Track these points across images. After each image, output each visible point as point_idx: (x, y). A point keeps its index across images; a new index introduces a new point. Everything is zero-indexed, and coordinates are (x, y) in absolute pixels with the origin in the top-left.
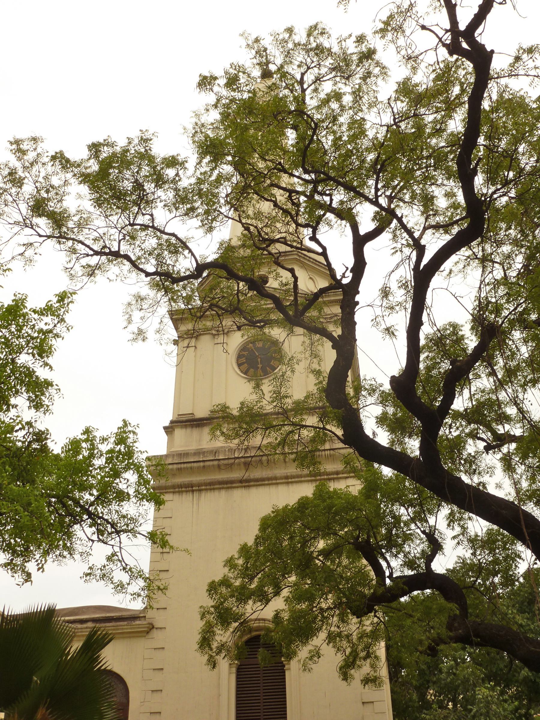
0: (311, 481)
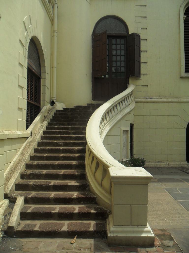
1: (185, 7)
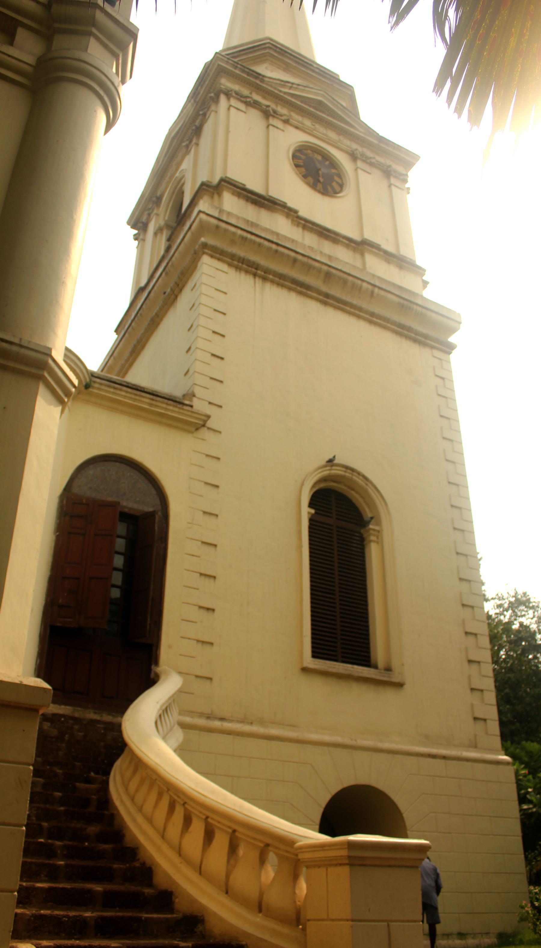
0: (195, 413)
1: (313, 487)
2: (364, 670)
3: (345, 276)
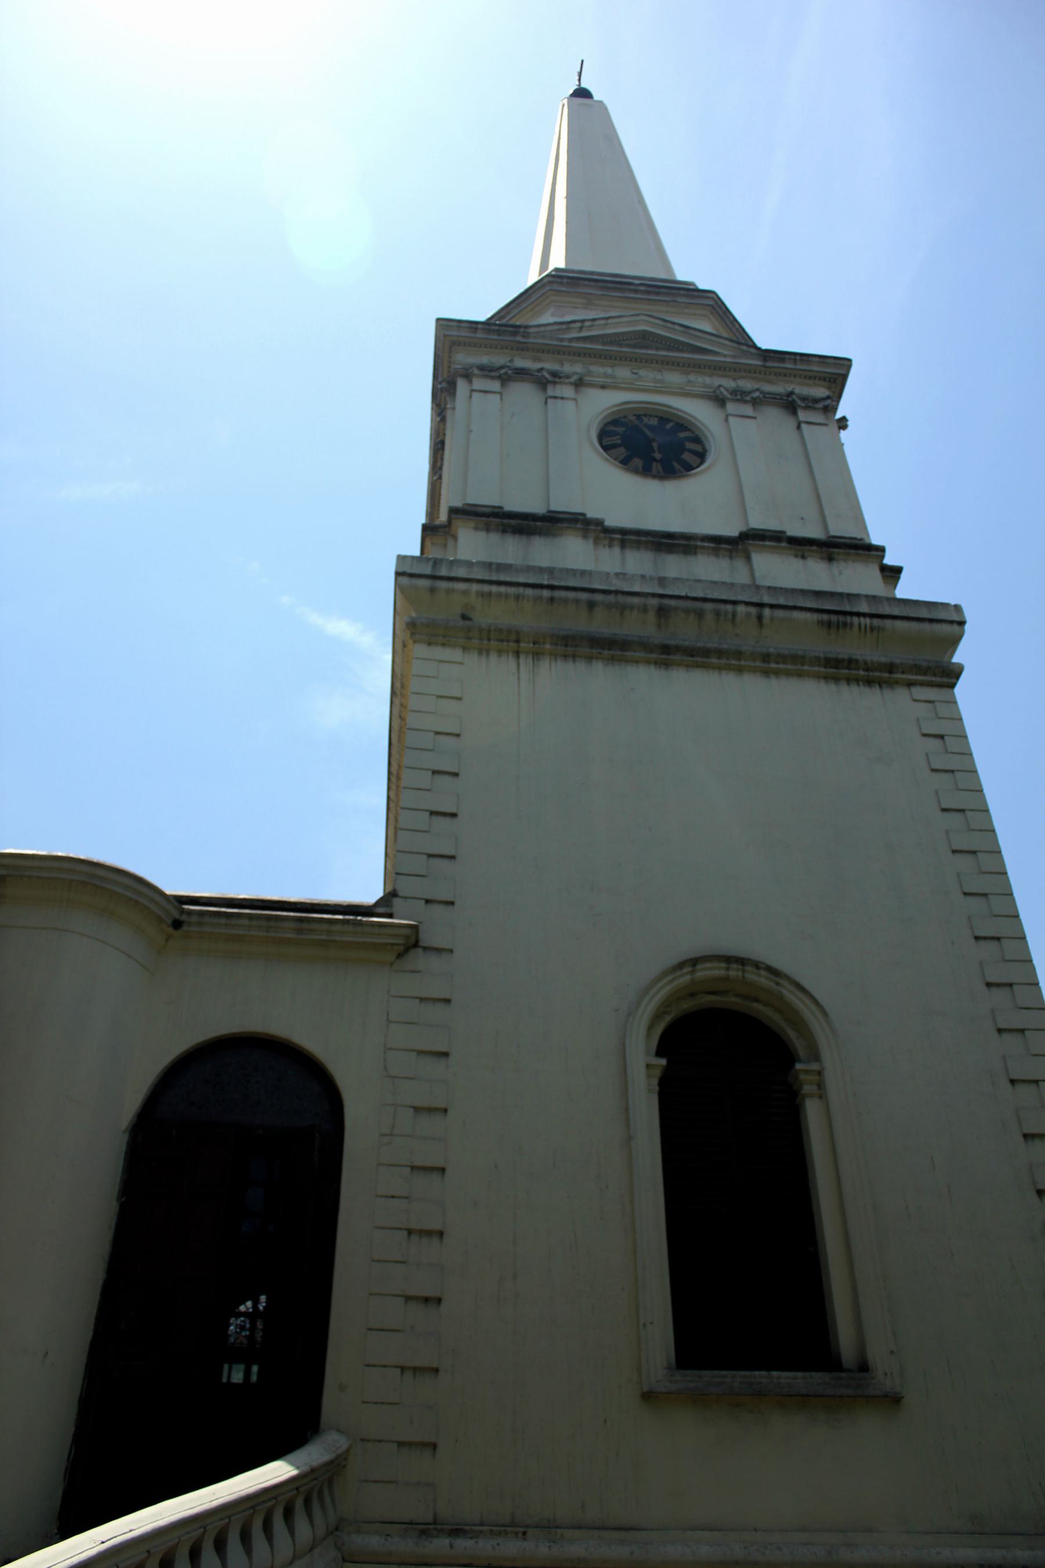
2: (796, 1378)
3: (698, 604)
